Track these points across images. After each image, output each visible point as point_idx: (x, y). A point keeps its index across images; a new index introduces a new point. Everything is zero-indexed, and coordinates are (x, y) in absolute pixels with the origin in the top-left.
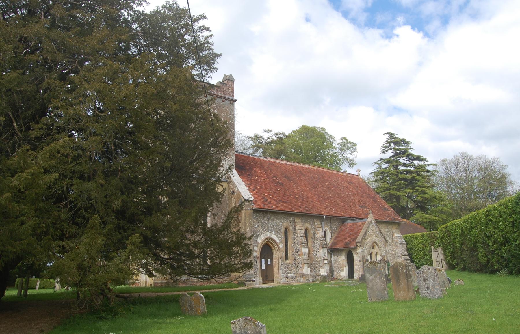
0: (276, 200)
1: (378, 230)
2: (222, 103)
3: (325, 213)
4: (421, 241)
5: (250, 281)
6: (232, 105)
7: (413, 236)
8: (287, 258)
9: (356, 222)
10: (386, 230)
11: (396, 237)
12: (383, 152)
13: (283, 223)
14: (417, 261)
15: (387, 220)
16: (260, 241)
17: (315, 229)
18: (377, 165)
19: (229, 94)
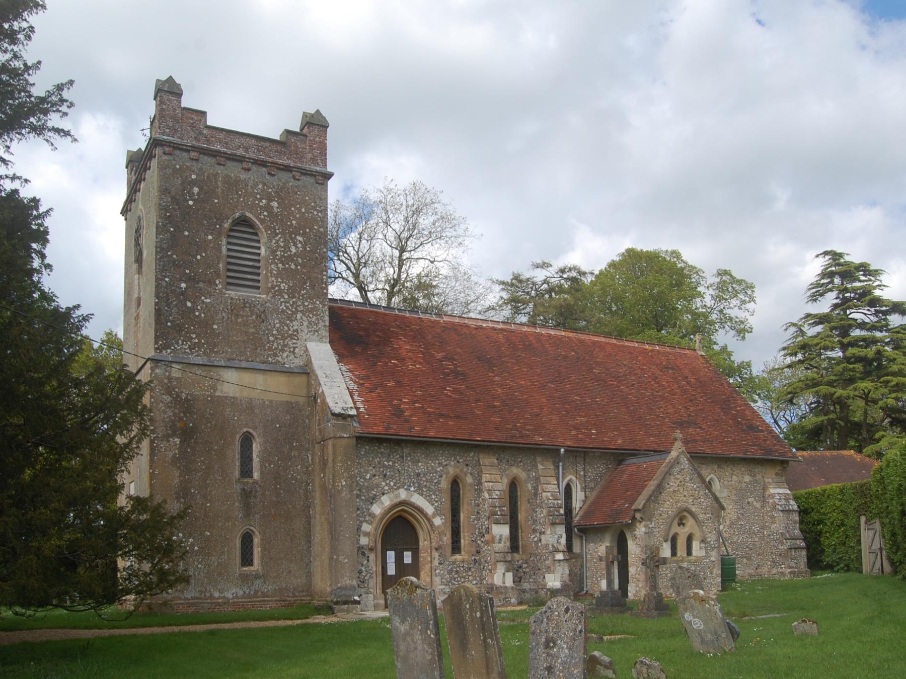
0: (430, 414)
1: (698, 480)
2: (292, 183)
3: (566, 441)
4: (838, 503)
5: (346, 603)
6: (319, 187)
7: (825, 491)
8: (456, 548)
9: (644, 462)
10: (747, 478)
11: (773, 496)
12: (814, 298)
13: (444, 468)
15: (749, 455)
16: (377, 510)
17: (537, 479)
18: (793, 329)
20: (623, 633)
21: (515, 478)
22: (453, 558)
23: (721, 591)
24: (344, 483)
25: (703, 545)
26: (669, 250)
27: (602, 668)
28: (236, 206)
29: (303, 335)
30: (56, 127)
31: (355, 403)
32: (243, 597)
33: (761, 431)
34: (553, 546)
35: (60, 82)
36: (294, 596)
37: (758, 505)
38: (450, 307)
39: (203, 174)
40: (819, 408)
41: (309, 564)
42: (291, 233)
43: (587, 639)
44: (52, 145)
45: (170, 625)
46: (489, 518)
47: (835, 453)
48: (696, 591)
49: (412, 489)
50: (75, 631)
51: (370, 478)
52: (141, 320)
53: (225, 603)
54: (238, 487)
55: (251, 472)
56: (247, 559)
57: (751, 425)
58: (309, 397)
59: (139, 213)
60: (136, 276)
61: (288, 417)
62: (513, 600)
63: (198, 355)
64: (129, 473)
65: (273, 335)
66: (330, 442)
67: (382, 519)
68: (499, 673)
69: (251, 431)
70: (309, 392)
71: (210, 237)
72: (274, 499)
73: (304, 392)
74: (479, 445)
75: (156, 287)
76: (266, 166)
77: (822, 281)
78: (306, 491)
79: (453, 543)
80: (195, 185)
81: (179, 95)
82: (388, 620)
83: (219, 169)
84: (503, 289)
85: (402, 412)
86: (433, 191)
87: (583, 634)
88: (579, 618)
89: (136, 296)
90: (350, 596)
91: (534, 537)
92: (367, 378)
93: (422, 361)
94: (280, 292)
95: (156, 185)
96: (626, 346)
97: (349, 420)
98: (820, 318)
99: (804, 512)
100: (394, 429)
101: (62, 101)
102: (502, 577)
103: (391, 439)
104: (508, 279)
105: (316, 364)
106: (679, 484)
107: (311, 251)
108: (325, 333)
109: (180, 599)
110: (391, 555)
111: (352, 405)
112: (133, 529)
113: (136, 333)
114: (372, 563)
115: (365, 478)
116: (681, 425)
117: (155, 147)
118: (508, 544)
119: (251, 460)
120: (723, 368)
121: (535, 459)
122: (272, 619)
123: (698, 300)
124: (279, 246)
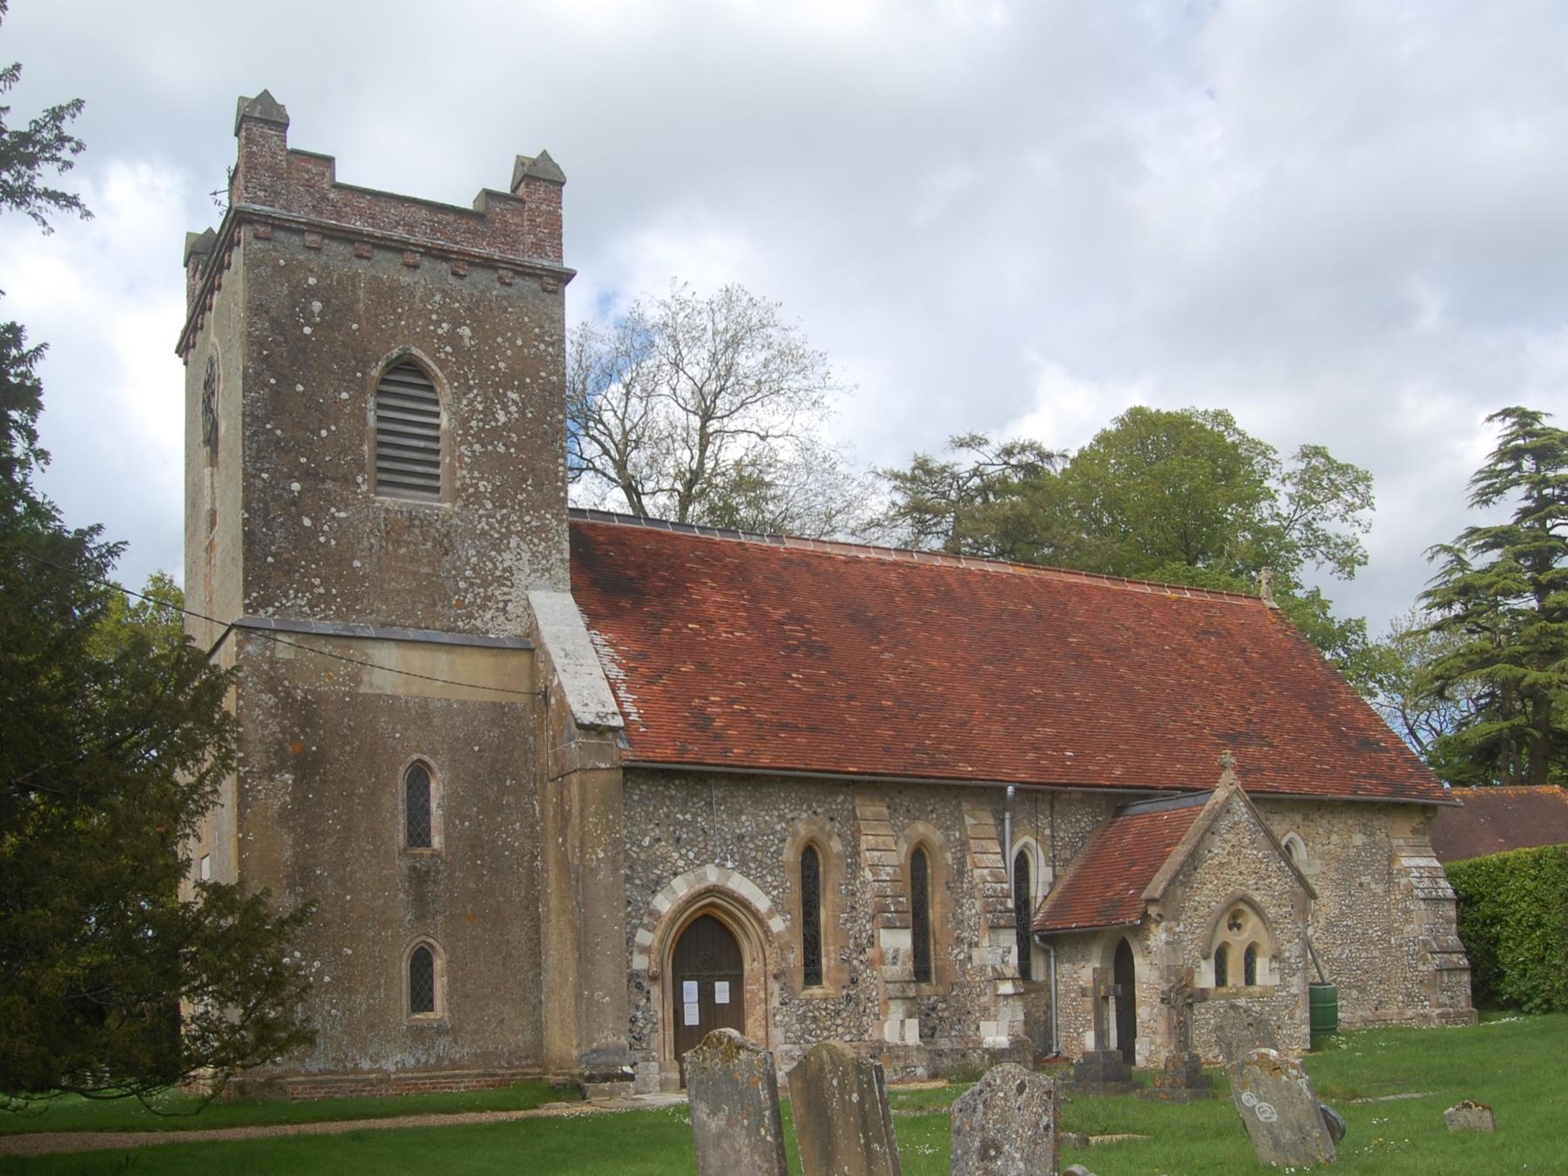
0: (761, 723)
2: (497, 291)
3: (1016, 771)
4: (1530, 885)
5: (607, 1078)
6: (549, 298)
7: (1505, 861)
8: (812, 975)
9: (1164, 810)
10: (1359, 839)
11: (1406, 872)
12: (1484, 498)
13: (789, 824)
14: (1515, 974)
15: (1362, 796)
16: (664, 904)
17: (963, 844)
18: (1444, 558)
19: (538, 248)
20: (1127, 1130)
23: (1310, 1051)
24: (601, 855)
25: (1275, 965)
28: (393, 337)
29: (521, 578)
30: (50, 189)
31: (620, 704)
32: (416, 1069)
33: (1386, 750)
34: (994, 969)
35: (56, 105)
37: (1379, 889)
38: (797, 523)
39: (329, 275)
40: (1493, 707)
41: (537, 1007)
42: (496, 386)
43: (1058, 1142)
44: (45, 223)
45: (279, 1123)
46: (873, 917)
48: (1263, 1050)
49: (729, 864)
50: (102, 1135)
51: (651, 845)
53: (381, 1081)
54: (403, 865)
55: (428, 835)
56: (421, 998)
57: (1366, 738)
59: (211, 351)
60: (207, 471)
62: (920, 1071)
63: (326, 618)
64: (199, 839)
65: (466, 579)
66: (575, 778)
67: (673, 921)
69: (426, 758)
70: (534, 684)
71: (345, 395)
72: (471, 885)
73: (525, 685)
74: (853, 781)
75: (245, 489)
76: (446, 259)
77: (1500, 467)
78: (531, 870)
80: (314, 296)
82: (686, 1110)
83: (361, 267)
85: (709, 720)
86: (764, 304)
87: (1051, 1133)
88: (1044, 1103)
89: (208, 507)
90: (615, 1066)
92: (643, 656)
93: (745, 624)
94: (478, 498)
95: (241, 298)
97: (610, 735)
98: (1496, 536)
99: (1465, 901)
100: (694, 751)
101: (62, 139)
102: (898, 1028)
103: (689, 772)
104: (906, 468)
105: (547, 632)
106: (1229, 850)
108: (563, 573)
111: (616, 709)
112: (209, 943)
113: (208, 577)
115: (640, 846)
116: (1233, 739)
117: (239, 225)
118: (910, 965)
119: (428, 812)
120: (1313, 630)
121: (960, 804)
122: (470, 1110)
124: (474, 411)
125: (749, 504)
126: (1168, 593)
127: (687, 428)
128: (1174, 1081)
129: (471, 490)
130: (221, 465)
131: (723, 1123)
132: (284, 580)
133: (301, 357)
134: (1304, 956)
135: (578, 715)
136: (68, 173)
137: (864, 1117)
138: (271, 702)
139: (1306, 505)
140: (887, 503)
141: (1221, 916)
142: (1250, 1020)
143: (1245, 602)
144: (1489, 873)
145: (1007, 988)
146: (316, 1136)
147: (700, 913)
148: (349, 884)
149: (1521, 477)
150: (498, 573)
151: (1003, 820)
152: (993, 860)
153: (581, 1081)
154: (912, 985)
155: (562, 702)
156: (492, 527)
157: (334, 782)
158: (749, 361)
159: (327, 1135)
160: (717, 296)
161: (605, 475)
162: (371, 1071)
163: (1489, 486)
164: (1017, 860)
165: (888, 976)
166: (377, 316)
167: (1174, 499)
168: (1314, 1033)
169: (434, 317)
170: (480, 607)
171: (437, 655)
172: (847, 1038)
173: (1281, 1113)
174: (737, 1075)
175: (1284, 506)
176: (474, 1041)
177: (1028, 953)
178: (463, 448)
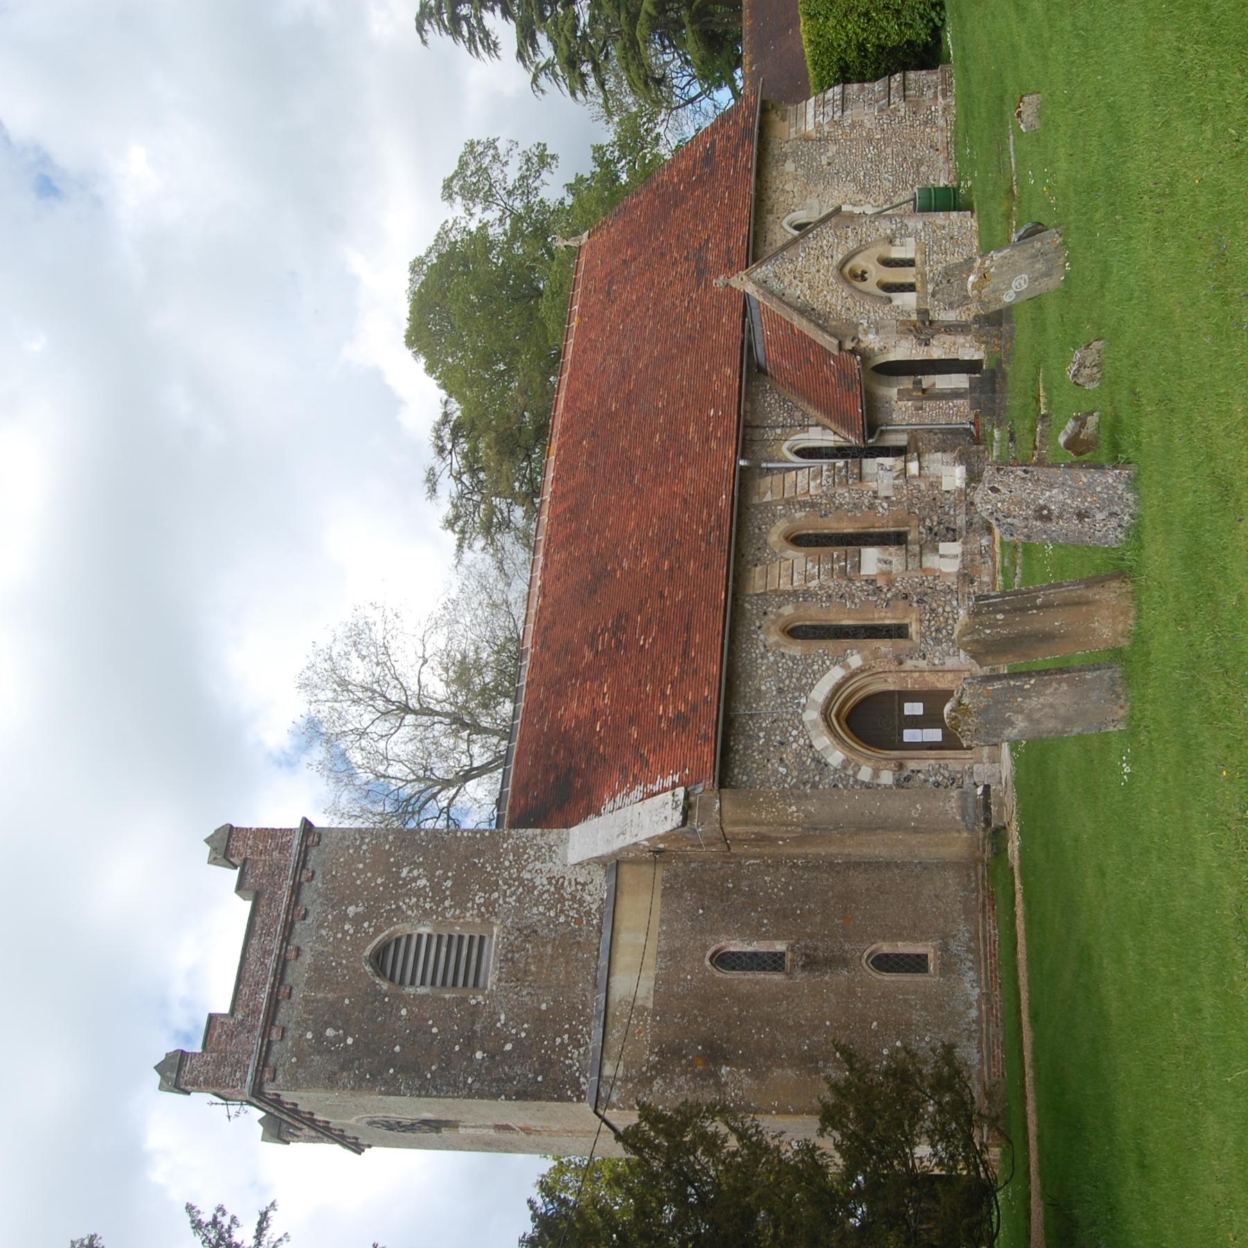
0: (682, 672)
1: (792, 251)
2: (318, 883)
3: (726, 457)
4: (832, 22)
5: (987, 808)
6: (325, 840)
7: (811, 41)
8: (899, 632)
10: (790, 166)
11: (818, 126)
12: (492, 47)
13: (769, 649)
15: (753, 165)
16: (836, 757)
17: (788, 502)
19: (283, 848)
20: (1036, 381)
21: (786, 538)
22: (914, 637)
23: (972, 212)
24: (794, 808)
25: (897, 242)
26: (409, 276)
27: (1084, 431)
28: (355, 970)
29: (557, 870)
30: (254, 1233)
31: (665, 790)
32: (978, 971)
33: (713, 144)
34: (897, 478)
35: (190, 1225)
36: (976, 890)
37: (833, 149)
38: (499, 633)
39: (305, 1021)
40: (669, 31)
41: (925, 867)
42: (397, 886)
43: (1041, 463)
44: (280, 1240)
45: (1024, 1086)
46: (850, 580)
47: (746, 12)
48: (969, 286)
49: (803, 701)
50: (1033, 1235)
51: (786, 766)
52: (532, 1124)
53: (988, 1001)
54: (800, 976)
55: (775, 954)
56: (917, 964)
57: (703, 156)
58: (655, 861)
59: (363, 1124)
60: (462, 1131)
61: (687, 895)
62: (984, 542)
63: (589, 1034)
64: (783, 1132)
65: (557, 916)
66: (728, 829)
67: (851, 749)
68: (1087, 587)
69: (709, 954)
70: (646, 862)
71: (404, 1012)
72: (818, 919)
73: (647, 870)
74: (733, 595)
75: (481, 1097)
76: (292, 924)
77: (465, 33)
78: (805, 868)
79: (891, 637)
80: (322, 1034)
81: (182, 1056)
82: (1014, 746)
83: (298, 995)
84: (470, 547)
85: (679, 715)
86: (312, 658)
87: (1029, 469)
88: (1007, 474)
89: (492, 1132)
90: (977, 801)
91: (882, 508)
92: (624, 770)
93: (597, 683)
94: (489, 904)
95: (322, 1094)
96: (574, 357)
97: (692, 799)
98: (525, 37)
99: (845, 75)
100: (707, 728)
101: (215, 1223)
102: (947, 559)
103: (724, 733)
104: (452, 538)
105: (603, 849)
106: (798, 280)
107: (424, 854)
108: (553, 835)
109: (981, 1071)
110: (909, 735)
111: (669, 793)
112: (869, 1129)
113: (551, 1133)
114: (924, 765)
115: (786, 776)
116: (702, 273)
117: (263, 1094)
118: (892, 549)
119: (755, 954)
120: (601, 194)
121: (756, 506)
122: (1014, 924)
123: (491, 231)
124: (417, 905)
125: (480, 673)
126: (574, 324)
127: (416, 726)
128: (996, 336)
129: (483, 909)
130: (459, 1118)
131: (1020, 717)
132: (557, 1068)
133: (372, 1047)
134: (890, 217)
135: (674, 825)
136: (240, 1220)
137: (1016, 610)
138: (660, 1082)
139: (493, 196)
140: (483, 555)
141: (854, 288)
142: (944, 282)
143: (583, 259)
144: (821, 54)
145: (913, 467)
146: (1034, 1052)
147: (845, 726)
148: (816, 1022)
149: (476, 16)
150: (552, 889)
151: (768, 469)
152: (802, 478)
153: (989, 830)
154: (910, 547)
155: (662, 838)
156: (513, 894)
157: (729, 1032)
158: (359, 672)
159: (1033, 1043)
160: (304, 696)
161: (454, 797)
162: (979, 1009)
163: (482, 43)
164: (803, 457)
165: (901, 568)
166: (338, 983)
167: (488, 310)
168: (957, 208)
169: (339, 936)
170: (581, 905)
171: (621, 942)
172: (955, 603)
173: (1020, 272)
174: (981, 706)
175: (493, 214)
176: (954, 921)
177: (883, 448)
178: (448, 915)
